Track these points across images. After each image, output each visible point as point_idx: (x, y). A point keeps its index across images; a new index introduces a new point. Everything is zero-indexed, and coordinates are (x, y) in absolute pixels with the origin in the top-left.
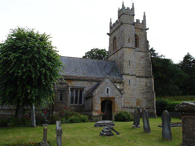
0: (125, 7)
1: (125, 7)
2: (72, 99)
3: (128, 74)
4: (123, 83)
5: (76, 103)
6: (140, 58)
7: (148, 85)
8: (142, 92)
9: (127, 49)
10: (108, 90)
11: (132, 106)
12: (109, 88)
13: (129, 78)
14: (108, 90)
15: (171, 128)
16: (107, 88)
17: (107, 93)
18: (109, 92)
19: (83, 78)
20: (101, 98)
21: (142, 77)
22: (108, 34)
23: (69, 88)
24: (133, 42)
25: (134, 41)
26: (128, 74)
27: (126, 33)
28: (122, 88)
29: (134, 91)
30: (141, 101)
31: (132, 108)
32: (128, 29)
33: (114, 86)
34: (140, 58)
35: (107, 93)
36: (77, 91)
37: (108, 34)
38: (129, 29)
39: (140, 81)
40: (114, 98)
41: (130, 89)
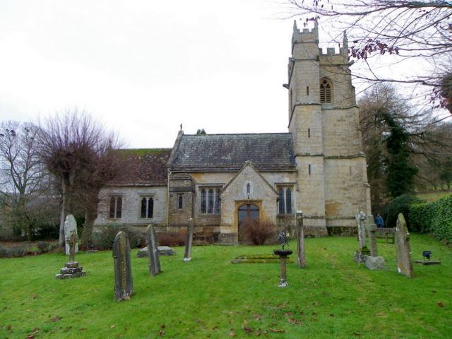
0: (299, 30)
1: (299, 30)
2: (203, 205)
3: (307, 155)
4: (297, 172)
5: (210, 212)
6: (336, 122)
7: (355, 171)
8: (342, 186)
9: (305, 108)
10: (248, 185)
11: (316, 214)
12: (250, 182)
13: (308, 161)
14: (248, 185)
15: (162, 258)
16: (247, 182)
17: (248, 191)
18: (252, 191)
19: (201, 169)
20: (237, 202)
21: (342, 158)
22: (284, 86)
23: (197, 186)
24: (316, 92)
25: (319, 90)
26: (307, 155)
27: (301, 79)
28: (294, 181)
29: (332, 184)
30: (341, 204)
31: (316, 217)
32: (318, 73)
33: (261, 179)
34: (336, 122)
35: (248, 191)
36: (211, 191)
37: (284, 86)
38: (308, 69)
39: (338, 166)
40: (261, 201)
41: (312, 182)
